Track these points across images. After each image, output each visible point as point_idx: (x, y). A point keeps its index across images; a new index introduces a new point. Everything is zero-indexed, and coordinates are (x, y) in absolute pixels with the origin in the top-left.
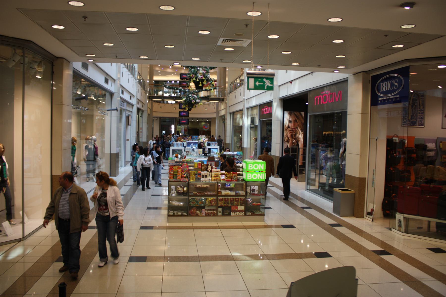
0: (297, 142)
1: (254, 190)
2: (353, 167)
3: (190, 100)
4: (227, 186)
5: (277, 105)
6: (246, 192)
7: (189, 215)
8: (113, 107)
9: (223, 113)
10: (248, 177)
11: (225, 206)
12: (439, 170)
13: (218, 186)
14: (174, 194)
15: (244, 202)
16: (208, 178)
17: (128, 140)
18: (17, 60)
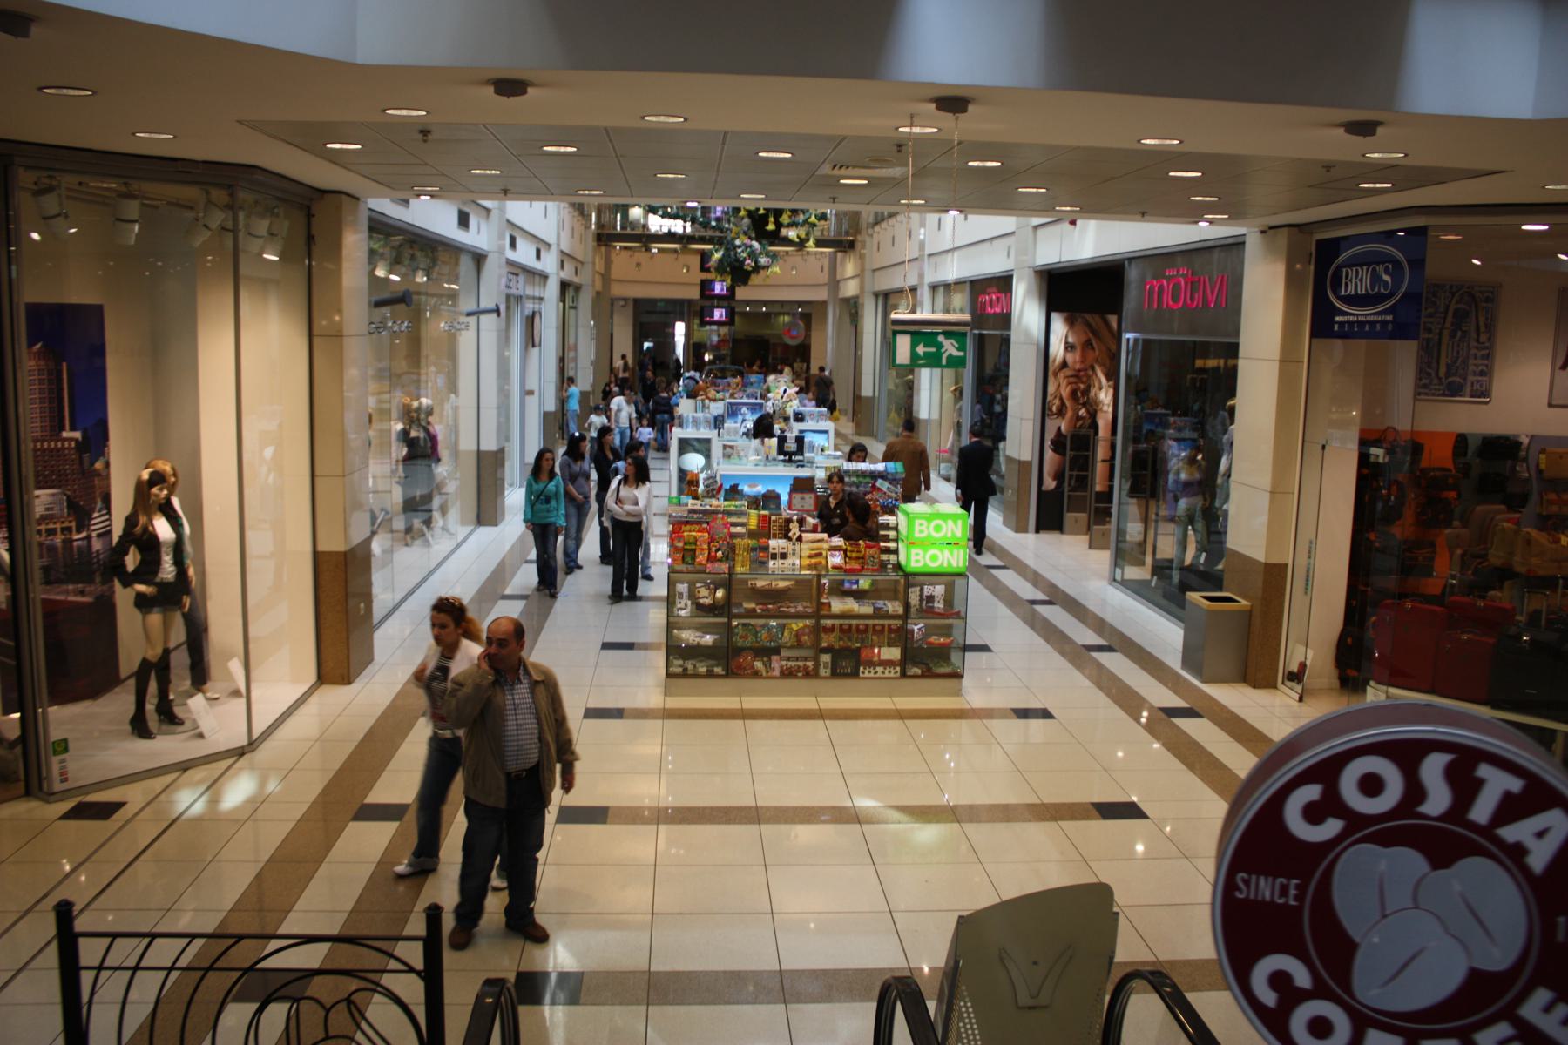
0: (1093, 415)
1: (931, 598)
2: (1249, 529)
3: (737, 260)
4: (847, 585)
5: (1028, 292)
6: (907, 606)
7: (730, 673)
8: (486, 303)
9: (850, 289)
10: (915, 559)
11: (842, 649)
12: (1528, 542)
13: (820, 587)
14: (684, 610)
15: (901, 636)
16: (789, 561)
17: (531, 393)
18: (214, 225)
